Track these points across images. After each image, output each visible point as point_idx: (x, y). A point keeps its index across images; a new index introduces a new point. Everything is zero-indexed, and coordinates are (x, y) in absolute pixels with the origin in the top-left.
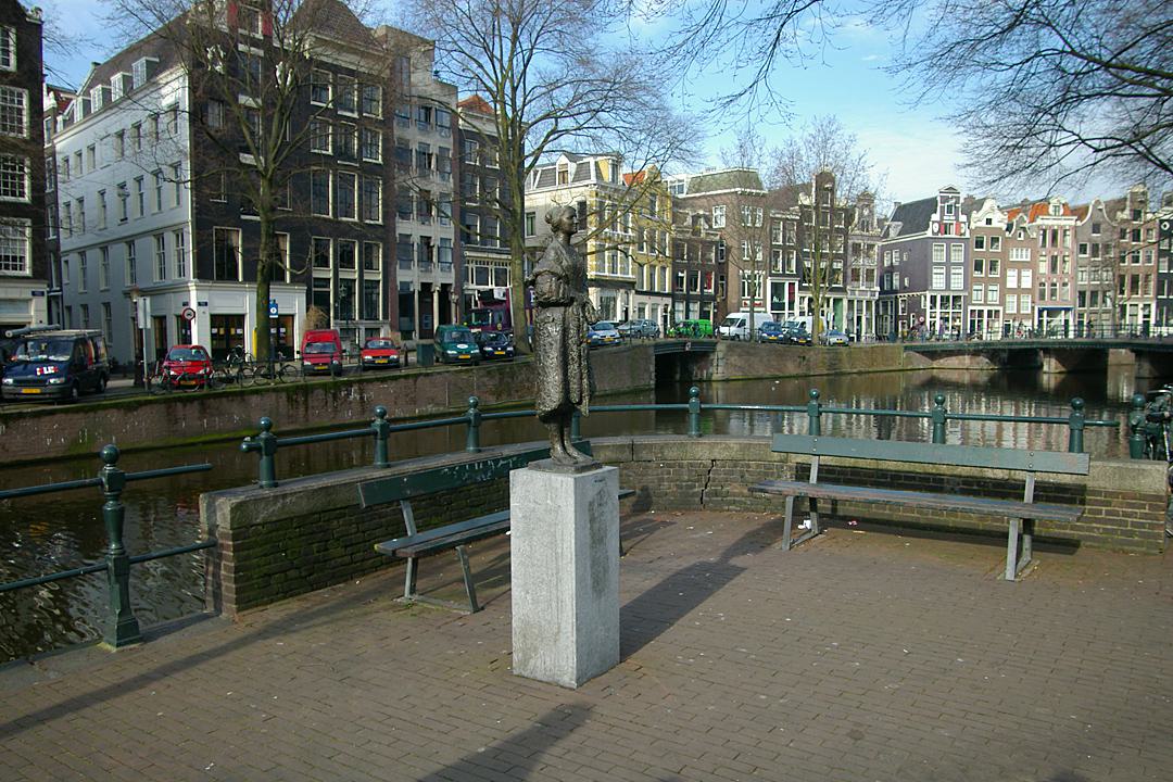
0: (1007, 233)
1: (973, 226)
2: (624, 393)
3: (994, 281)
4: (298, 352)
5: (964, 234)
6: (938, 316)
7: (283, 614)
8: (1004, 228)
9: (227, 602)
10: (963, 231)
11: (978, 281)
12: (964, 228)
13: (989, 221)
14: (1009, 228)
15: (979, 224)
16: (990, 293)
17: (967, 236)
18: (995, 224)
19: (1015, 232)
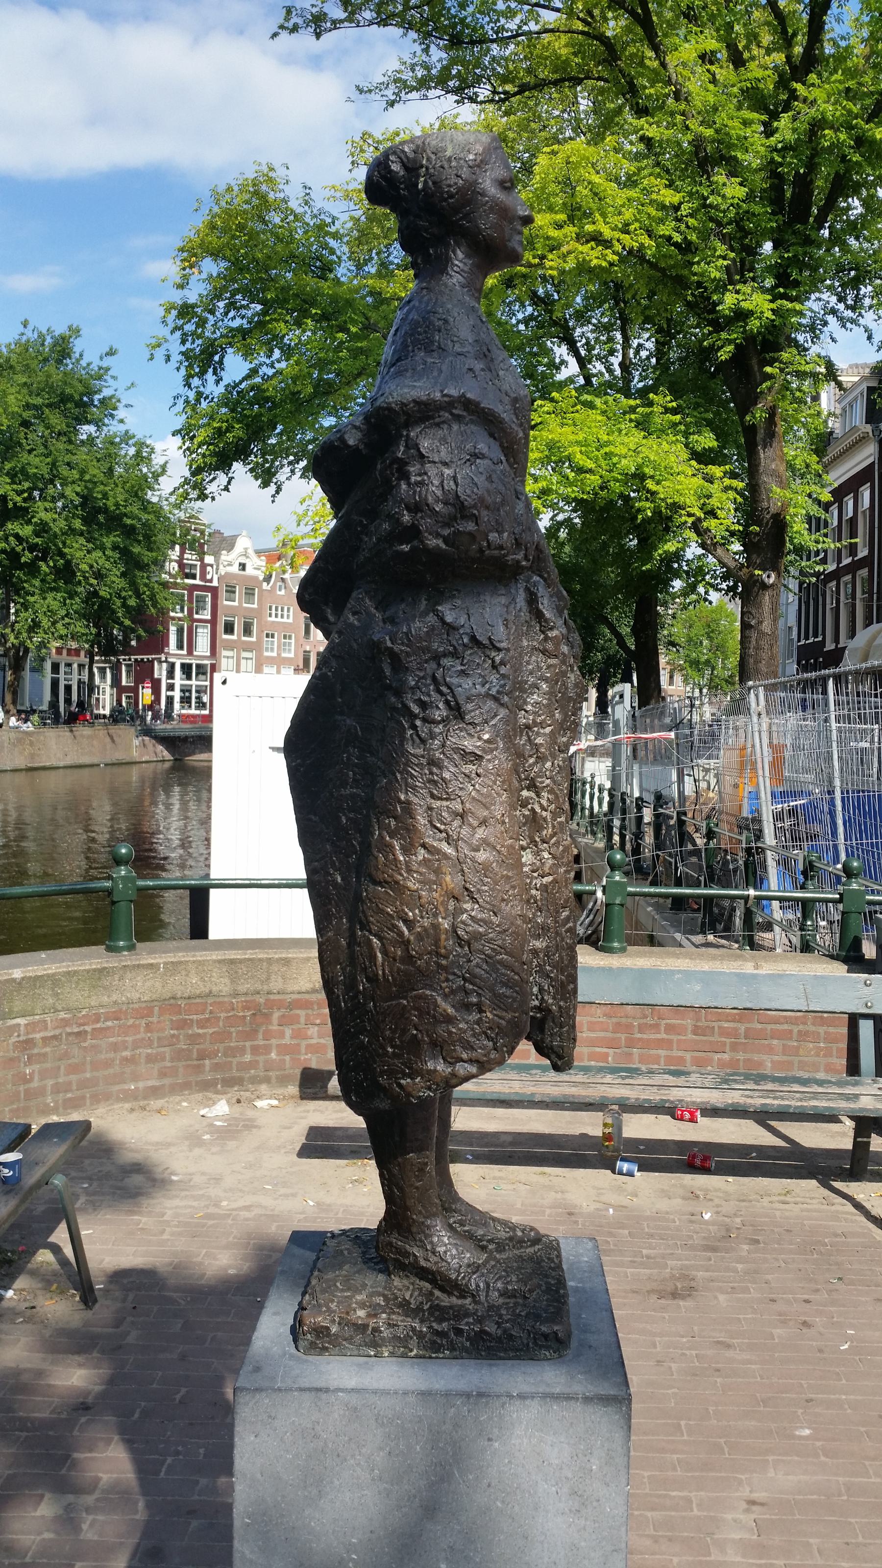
0: (265, 584)
1: (223, 571)
2: (21, 770)
3: (248, 648)
4: (237, 437)
5: (211, 581)
6: (177, 688)
7: (658, 1098)
8: (261, 578)
9: (367, 1147)
10: (209, 577)
11: (230, 646)
12: (210, 573)
13: (243, 567)
14: (268, 579)
15: (230, 569)
16: (243, 662)
17: (215, 583)
18: (249, 571)
19: (275, 583)
